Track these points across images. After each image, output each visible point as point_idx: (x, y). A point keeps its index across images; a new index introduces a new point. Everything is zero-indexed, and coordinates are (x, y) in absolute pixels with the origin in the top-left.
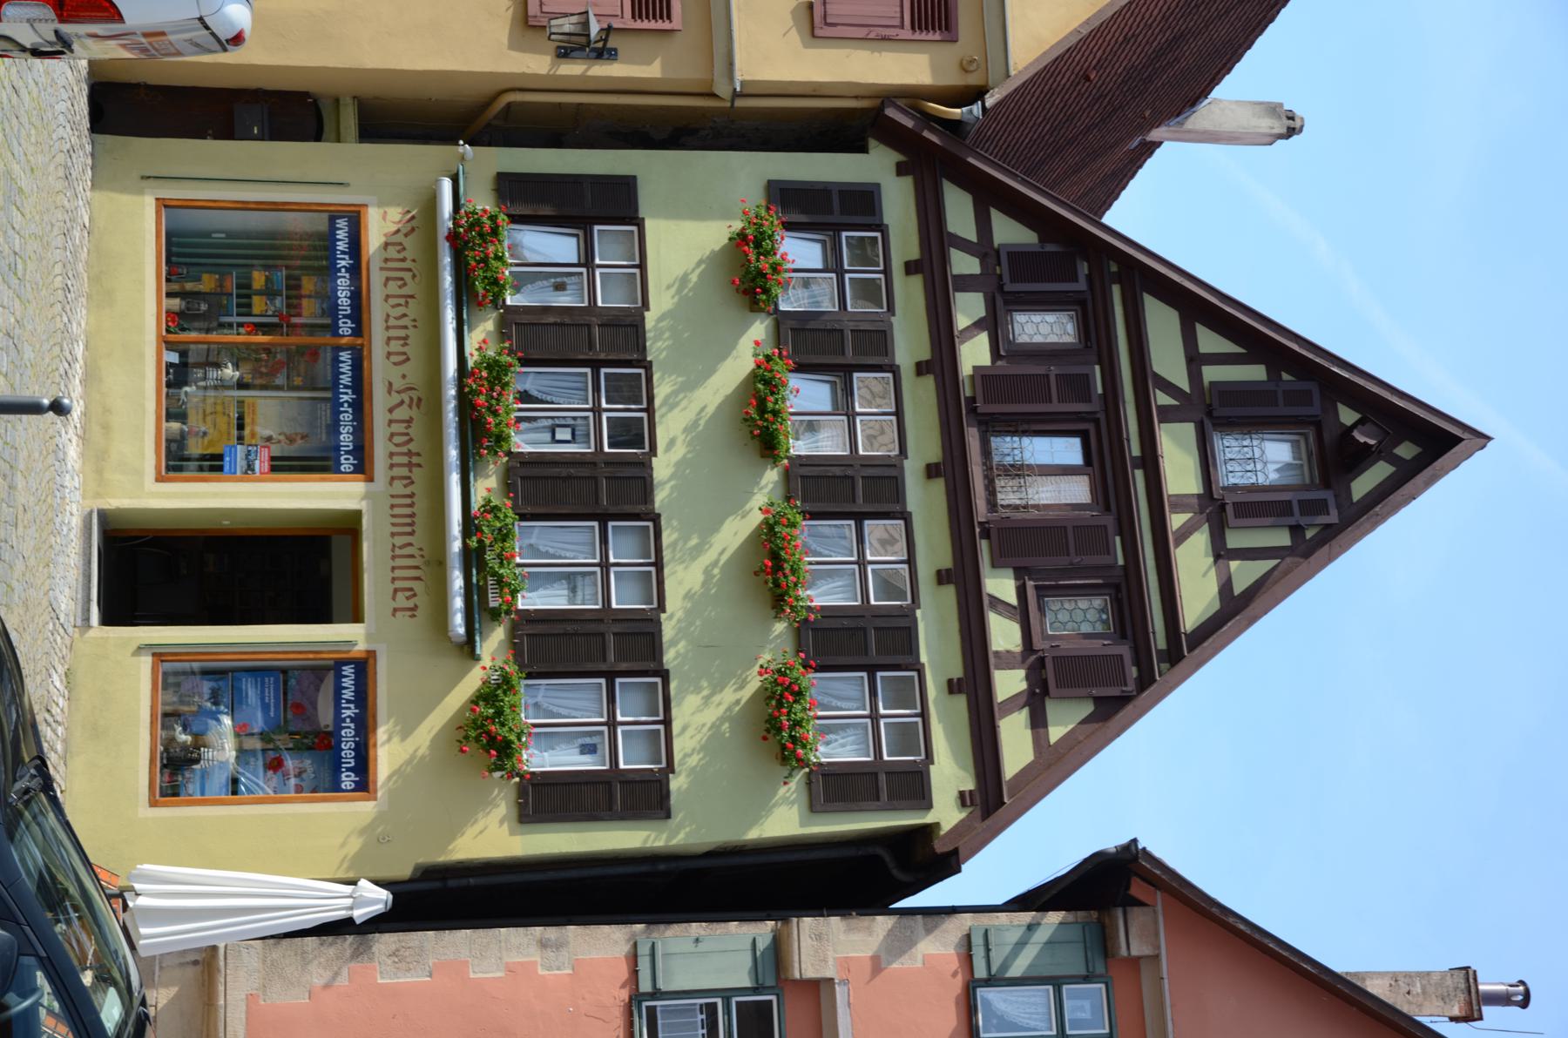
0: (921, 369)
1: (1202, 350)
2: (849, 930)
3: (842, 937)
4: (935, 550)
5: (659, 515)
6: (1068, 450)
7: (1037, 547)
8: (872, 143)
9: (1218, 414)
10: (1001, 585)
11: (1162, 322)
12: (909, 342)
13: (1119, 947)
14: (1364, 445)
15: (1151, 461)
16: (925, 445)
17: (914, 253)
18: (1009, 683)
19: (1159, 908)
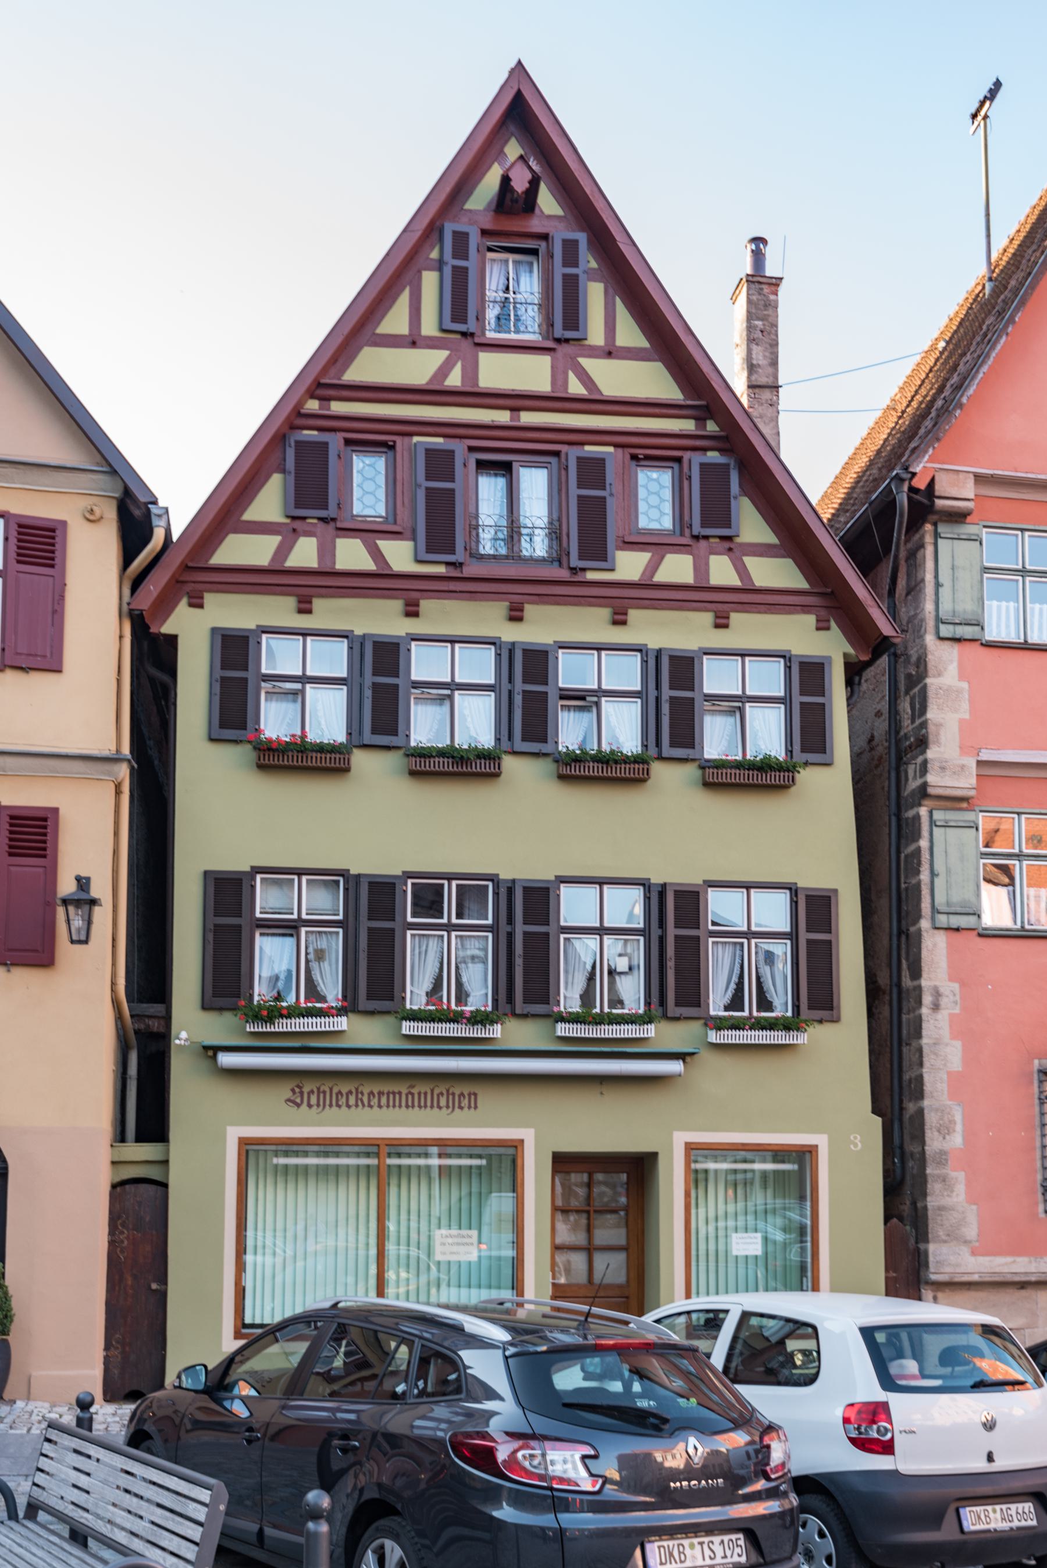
0: (412, 612)
2: (938, 743)
3: (942, 749)
4: (591, 623)
7: (591, 523)
8: (167, 629)
9: (462, 325)
10: (629, 565)
11: (371, 366)
12: (383, 619)
15: (516, 401)
16: (488, 619)
17: (290, 602)
18: (722, 571)
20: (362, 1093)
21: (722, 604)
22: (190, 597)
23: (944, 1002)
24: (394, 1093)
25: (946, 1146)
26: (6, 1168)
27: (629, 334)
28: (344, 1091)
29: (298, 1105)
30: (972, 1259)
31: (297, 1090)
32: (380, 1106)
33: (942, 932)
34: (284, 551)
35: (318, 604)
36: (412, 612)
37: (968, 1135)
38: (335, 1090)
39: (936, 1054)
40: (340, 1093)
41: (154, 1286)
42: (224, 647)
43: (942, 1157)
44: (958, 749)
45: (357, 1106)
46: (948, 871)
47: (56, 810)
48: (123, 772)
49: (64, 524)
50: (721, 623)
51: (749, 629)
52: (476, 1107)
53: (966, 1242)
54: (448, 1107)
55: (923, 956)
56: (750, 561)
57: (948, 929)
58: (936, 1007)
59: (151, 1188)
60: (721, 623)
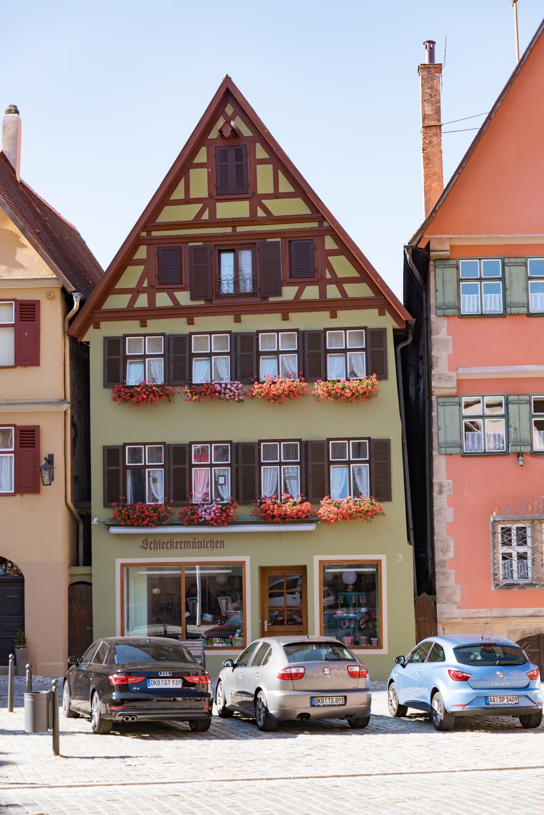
0: (191, 322)
1: (183, 198)
2: (437, 366)
3: (439, 369)
4: (273, 321)
5: (259, 440)
6: (227, 259)
8: (85, 339)
10: (289, 293)
11: (169, 214)
12: (178, 326)
13: (446, 254)
14: (230, 141)
15: (234, 223)
16: (225, 322)
17: (137, 323)
19: (430, 237)
20: (173, 542)
21: (333, 307)
22: (94, 325)
23: (444, 489)
24: (187, 542)
25: (445, 558)
26: (24, 579)
27: (285, 186)
28: (165, 542)
29: (146, 549)
30: (458, 611)
31: (145, 542)
32: (181, 548)
33: (443, 456)
34: (133, 301)
35: (149, 322)
36: (191, 322)
37: (456, 552)
38: (161, 541)
39: (440, 514)
40: (163, 542)
41: (88, 628)
42: (109, 346)
43: (443, 563)
44: (447, 369)
45: (171, 548)
46: (446, 427)
47: (38, 427)
48: (67, 407)
49: (39, 301)
50: (334, 316)
51: (347, 318)
52: (223, 547)
53: (455, 603)
54: (211, 547)
55: (434, 468)
56: (346, 286)
57: (446, 454)
58: (440, 492)
59: (85, 586)
60: (334, 316)
